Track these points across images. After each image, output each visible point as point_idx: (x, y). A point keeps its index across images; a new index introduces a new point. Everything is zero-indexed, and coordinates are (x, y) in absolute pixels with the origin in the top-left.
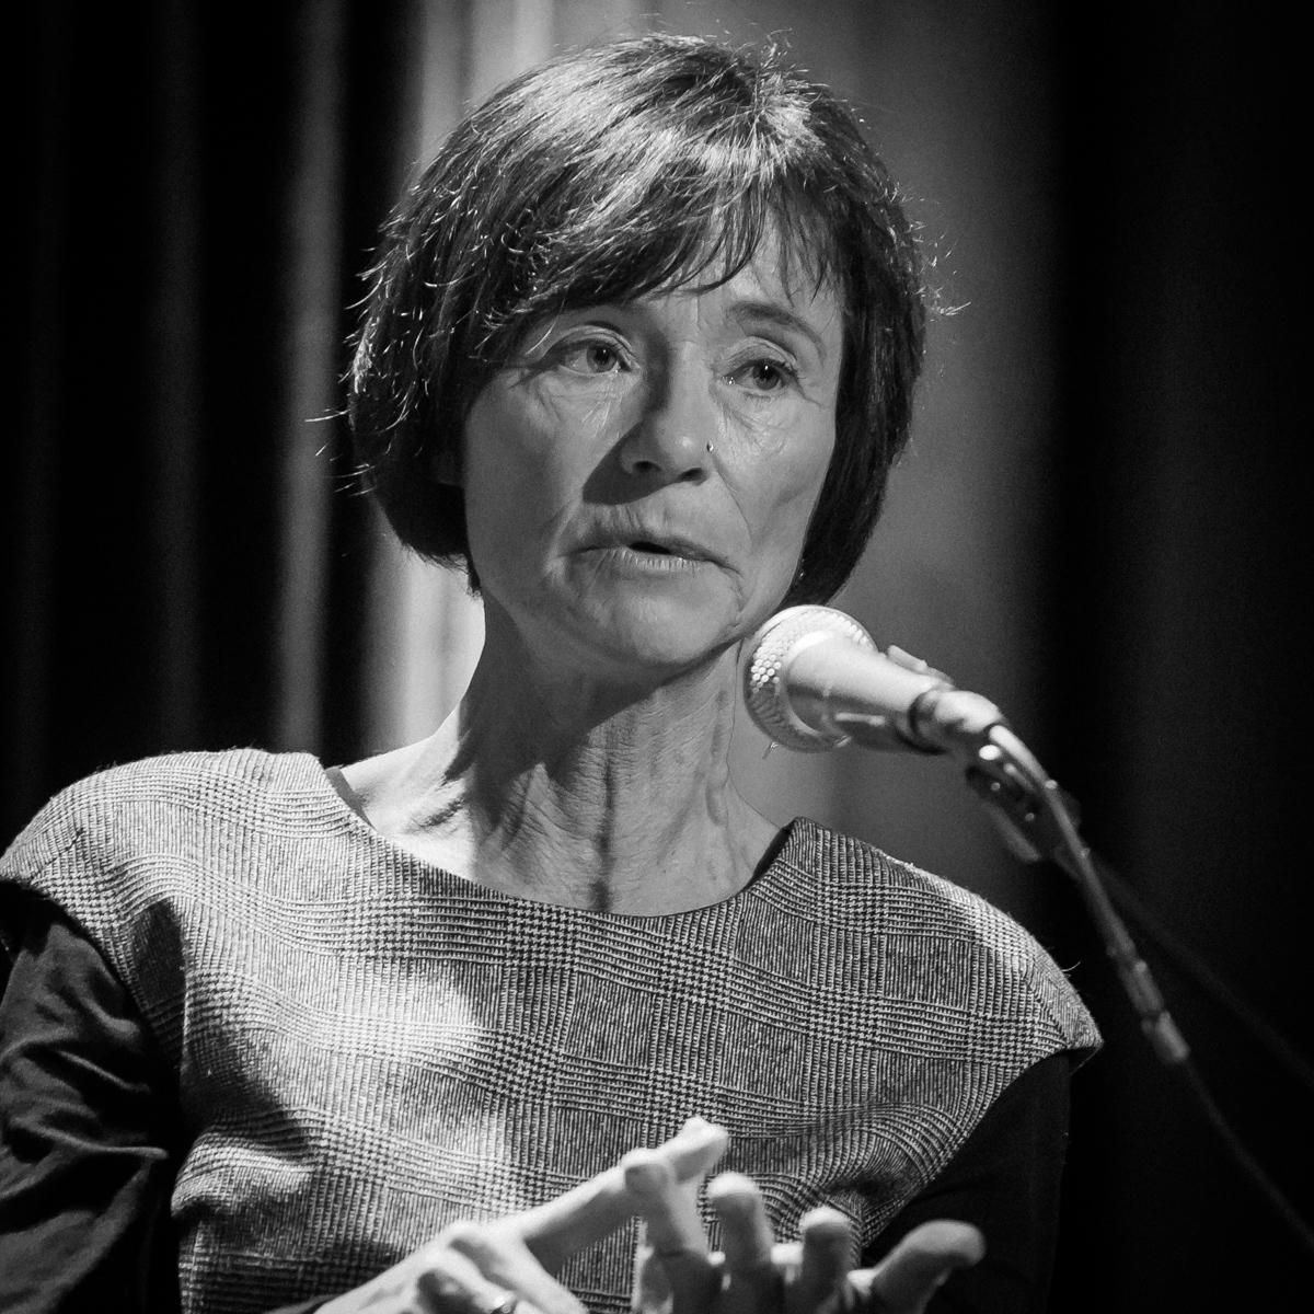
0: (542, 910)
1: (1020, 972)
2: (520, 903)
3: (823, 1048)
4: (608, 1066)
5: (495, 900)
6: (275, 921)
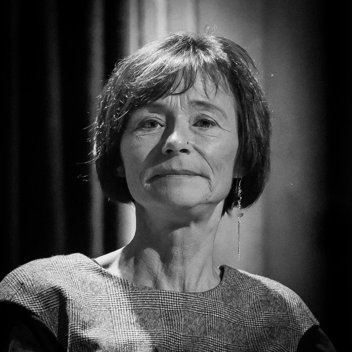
0: (169, 293)
1: (299, 303)
2: (162, 291)
3: (250, 329)
4: (195, 337)
5: (154, 291)
6: (88, 302)
